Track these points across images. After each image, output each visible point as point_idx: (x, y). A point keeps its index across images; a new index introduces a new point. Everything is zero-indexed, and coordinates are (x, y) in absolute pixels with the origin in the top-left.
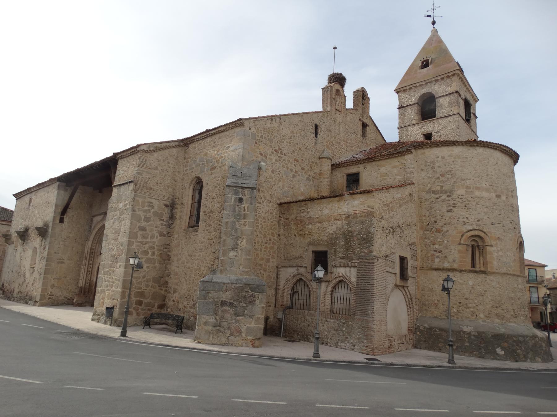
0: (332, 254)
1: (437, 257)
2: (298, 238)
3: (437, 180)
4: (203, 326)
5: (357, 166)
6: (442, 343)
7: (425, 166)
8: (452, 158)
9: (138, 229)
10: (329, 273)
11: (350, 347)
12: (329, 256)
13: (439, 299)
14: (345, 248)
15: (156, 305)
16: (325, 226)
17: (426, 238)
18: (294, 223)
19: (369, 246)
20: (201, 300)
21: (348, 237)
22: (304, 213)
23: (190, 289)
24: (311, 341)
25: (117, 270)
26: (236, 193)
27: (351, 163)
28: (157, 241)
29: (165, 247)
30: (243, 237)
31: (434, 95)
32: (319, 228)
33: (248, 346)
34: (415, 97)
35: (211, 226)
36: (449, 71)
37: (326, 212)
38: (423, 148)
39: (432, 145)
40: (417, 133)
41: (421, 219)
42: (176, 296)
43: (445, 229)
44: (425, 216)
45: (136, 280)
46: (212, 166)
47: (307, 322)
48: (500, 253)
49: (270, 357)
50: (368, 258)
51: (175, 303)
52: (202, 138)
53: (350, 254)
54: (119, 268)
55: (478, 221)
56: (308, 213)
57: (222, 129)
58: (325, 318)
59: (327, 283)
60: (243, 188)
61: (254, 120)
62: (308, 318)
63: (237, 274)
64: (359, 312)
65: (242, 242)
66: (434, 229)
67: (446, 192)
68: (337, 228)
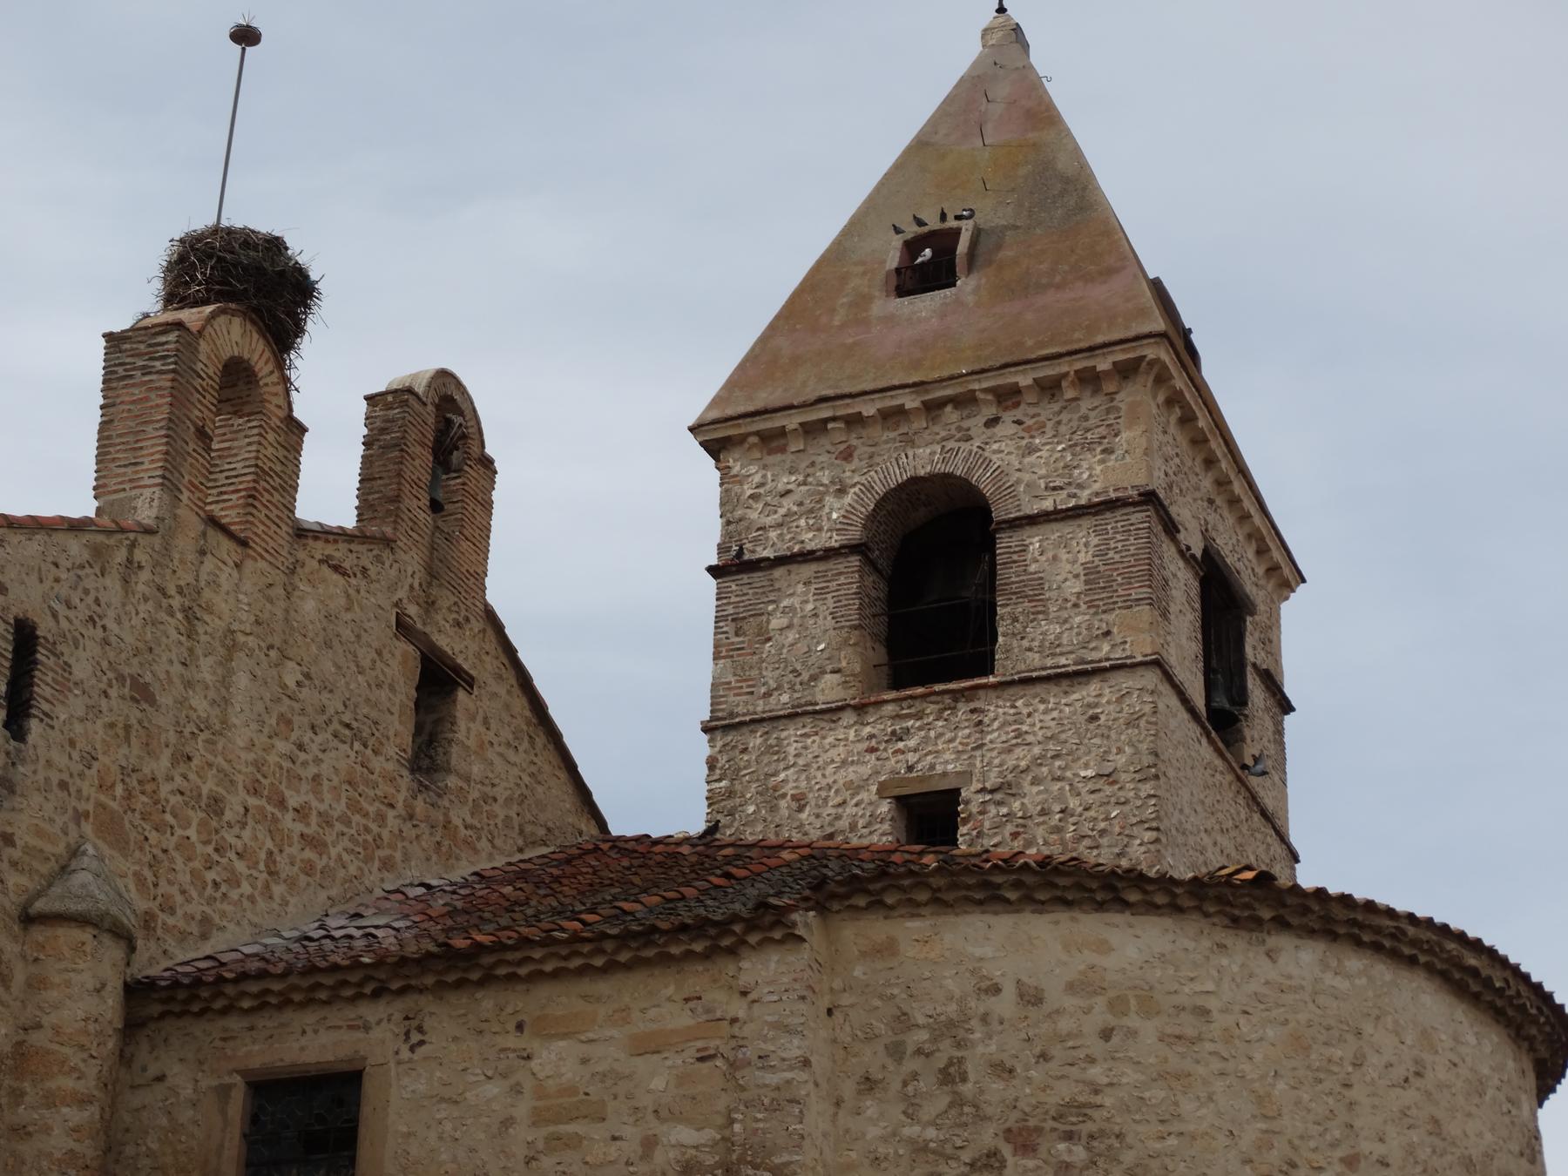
5: (350, 1013)
7: (896, 1051)
8: (1100, 1003)
34: (848, 499)
40: (849, 785)
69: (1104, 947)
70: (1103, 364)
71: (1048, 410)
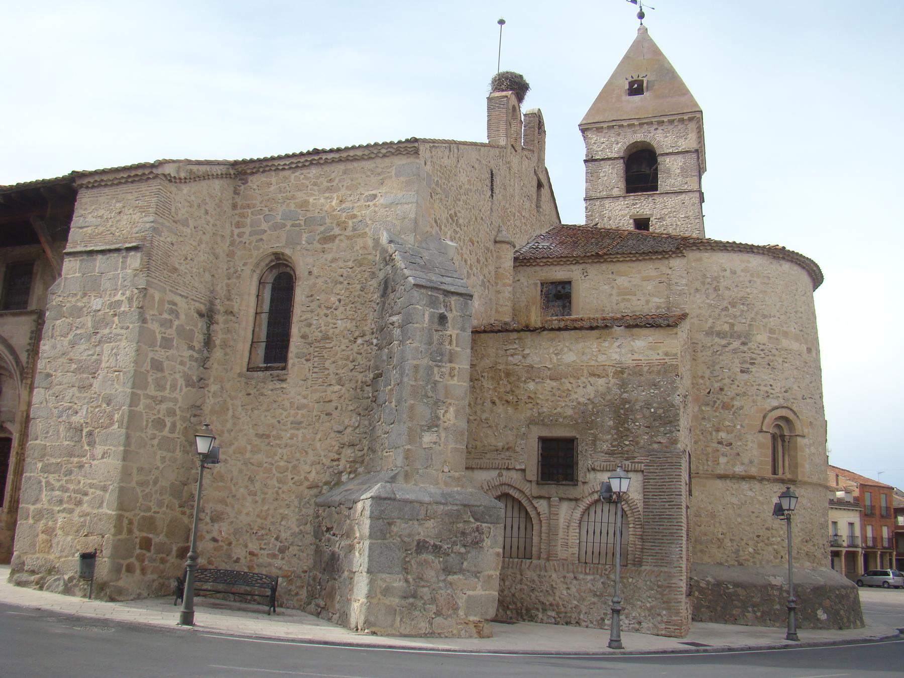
0: (587, 445)
1: (723, 455)
2: (500, 409)
3: (724, 313)
4: (382, 597)
5: (568, 267)
6: (739, 607)
7: (703, 283)
8: (748, 274)
9: (150, 364)
10: (580, 483)
11: (631, 626)
12: (580, 448)
13: (724, 531)
14: (615, 434)
15: (175, 548)
16: (569, 386)
17: (704, 418)
18: (490, 375)
19: (671, 432)
20: (375, 539)
21: (622, 411)
22: (516, 357)
23: (268, 515)
24: (539, 620)
25: (95, 462)
26: (433, 303)
27: (555, 259)
28: (181, 395)
29: (194, 412)
30: (449, 401)
31: (654, 148)
32: (554, 391)
33: (471, 637)
34: (619, 145)
35: (327, 372)
36: (685, 111)
37: (570, 357)
38: (699, 249)
39: (717, 246)
40: (622, 215)
41: (695, 382)
42: (223, 530)
43: (737, 403)
44: (703, 377)
45: (142, 489)
46: (322, 233)
47: (528, 583)
48: (813, 449)
49: (544, 654)
50: (668, 455)
51: (221, 546)
52: (294, 166)
53: (627, 445)
54: (103, 457)
55: (786, 392)
56: (524, 357)
57: (359, 153)
58: (573, 572)
59: (574, 503)
60: (447, 293)
61: (432, 145)
62: (529, 574)
63: (438, 484)
64: (650, 558)
65: (446, 412)
66: (719, 402)
67: (739, 337)
68: (597, 391)
69: (749, 262)
70: (686, 117)
71: (670, 127)
